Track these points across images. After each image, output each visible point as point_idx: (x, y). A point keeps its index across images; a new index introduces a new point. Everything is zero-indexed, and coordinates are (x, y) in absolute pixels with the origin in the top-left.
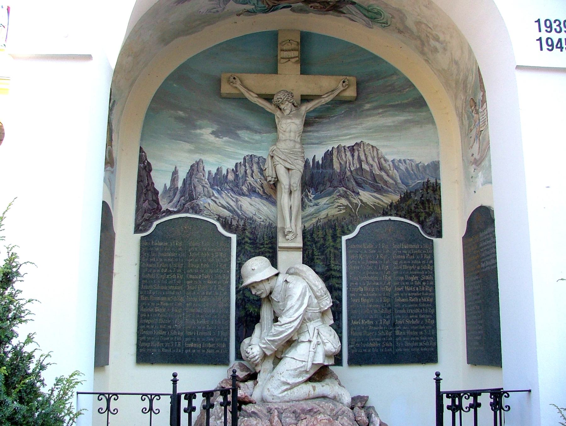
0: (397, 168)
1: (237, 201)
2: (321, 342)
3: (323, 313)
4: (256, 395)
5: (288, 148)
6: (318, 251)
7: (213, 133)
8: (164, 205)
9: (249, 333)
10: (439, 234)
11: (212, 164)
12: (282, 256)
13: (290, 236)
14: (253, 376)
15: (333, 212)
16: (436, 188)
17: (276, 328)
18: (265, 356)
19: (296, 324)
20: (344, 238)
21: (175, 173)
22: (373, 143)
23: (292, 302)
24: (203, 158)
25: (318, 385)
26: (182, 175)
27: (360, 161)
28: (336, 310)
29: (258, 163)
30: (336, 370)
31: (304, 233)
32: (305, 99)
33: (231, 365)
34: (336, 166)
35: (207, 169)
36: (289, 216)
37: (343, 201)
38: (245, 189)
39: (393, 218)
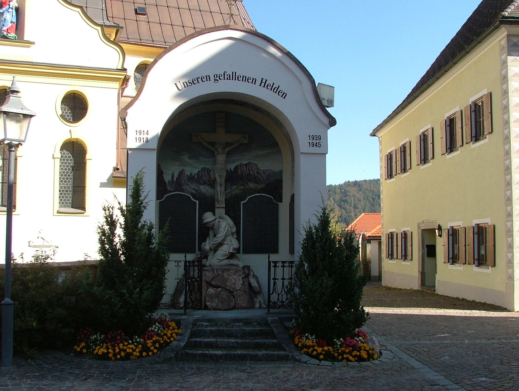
0: (264, 173)
1: (199, 187)
2: (231, 244)
3: (233, 234)
4: (208, 264)
5: (221, 165)
6: (232, 210)
7: (189, 158)
8: (169, 188)
9: (205, 241)
10: (282, 202)
11: (188, 171)
12: (217, 211)
13: (220, 203)
14: (206, 257)
15: (237, 192)
16: (281, 181)
17: (215, 239)
18: (211, 249)
19: (222, 238)
20: (242, 202)
21: (173, 175)
22: (255, 162)
23: (222, 229)
24: (185, 169)
25: (231, 261)
26: (176, 176)
27: (249, 170)
28: (238, 232)
29: (207, 171)
30: (238, 255)
31: (226, 200)
32: (228, 144)
33: (197, 253)
34: (239, 172)
35: (186, 173)
36: (220, 193)
37: (242, 187)
38: (202, 182)
39: (262, 194)
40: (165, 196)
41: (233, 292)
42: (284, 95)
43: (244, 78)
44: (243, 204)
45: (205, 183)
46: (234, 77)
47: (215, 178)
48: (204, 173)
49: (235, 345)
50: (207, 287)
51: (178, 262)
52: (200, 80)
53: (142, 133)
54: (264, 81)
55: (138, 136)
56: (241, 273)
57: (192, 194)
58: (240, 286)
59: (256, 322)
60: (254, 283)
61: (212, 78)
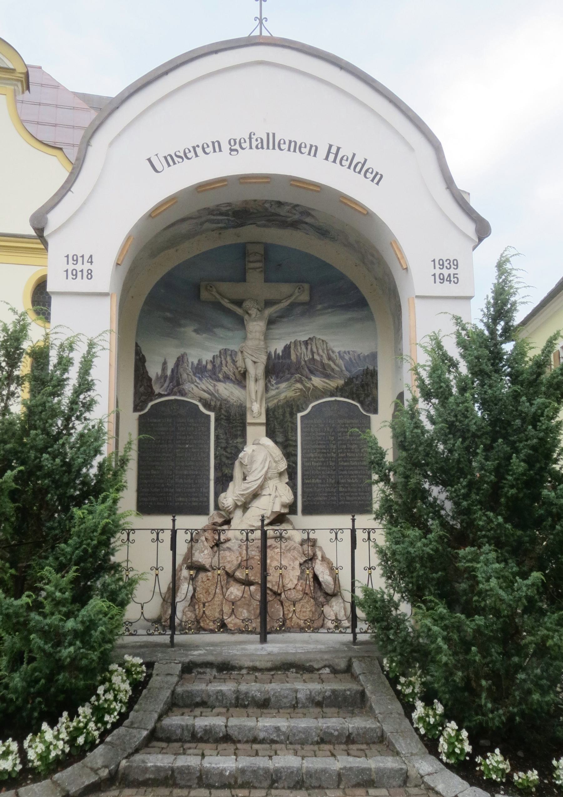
1: (215, 386)
6: (278, 426)
7: (196, 331)
8: (157, 389)
15: (290, 394)
19: (259, 482)
20: (299, 415)
21: (165, 363)
23: (257, 465)
26: (171, 366)
27: (313, 353)
28: (291, 472)
29: (231, 355)
31: (268, 411)
34: (293, 357)
35: (190, 360)
37: (299, 385)
38: (221, 376)
40: (150, 404)
41: (280, 595)
42: (377, 178)
43: (293, 144)
44: (302, 417)
45: (227, 378)
46: (271, 142)
47: (246, 368)
48: (225, 359)
49: (274, 736)
50: (228, 582)
51: (158, 531)
52: (199, 151)
53: (80, 260)
54: (334, 150)
55: (71, 267)
56: (295, 553)
57: (201, 400)
58: (296, 582)
59: (329, 666)
60: (325, 577)
61: (225, 147)
